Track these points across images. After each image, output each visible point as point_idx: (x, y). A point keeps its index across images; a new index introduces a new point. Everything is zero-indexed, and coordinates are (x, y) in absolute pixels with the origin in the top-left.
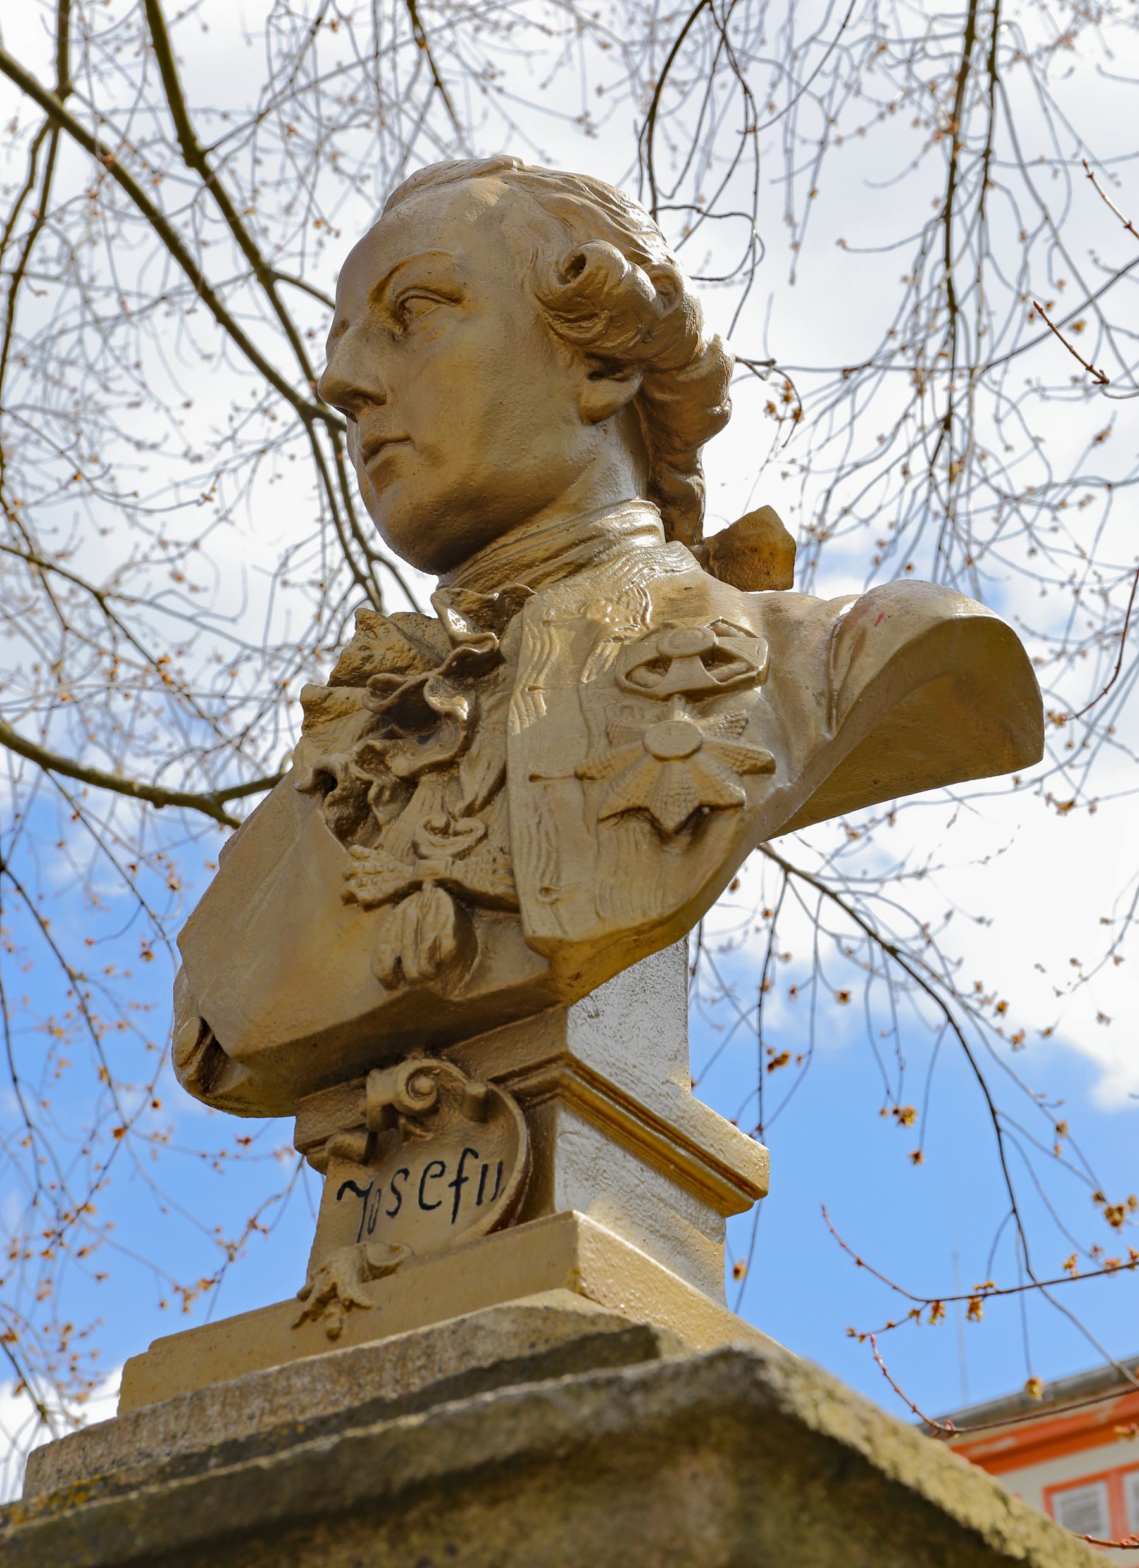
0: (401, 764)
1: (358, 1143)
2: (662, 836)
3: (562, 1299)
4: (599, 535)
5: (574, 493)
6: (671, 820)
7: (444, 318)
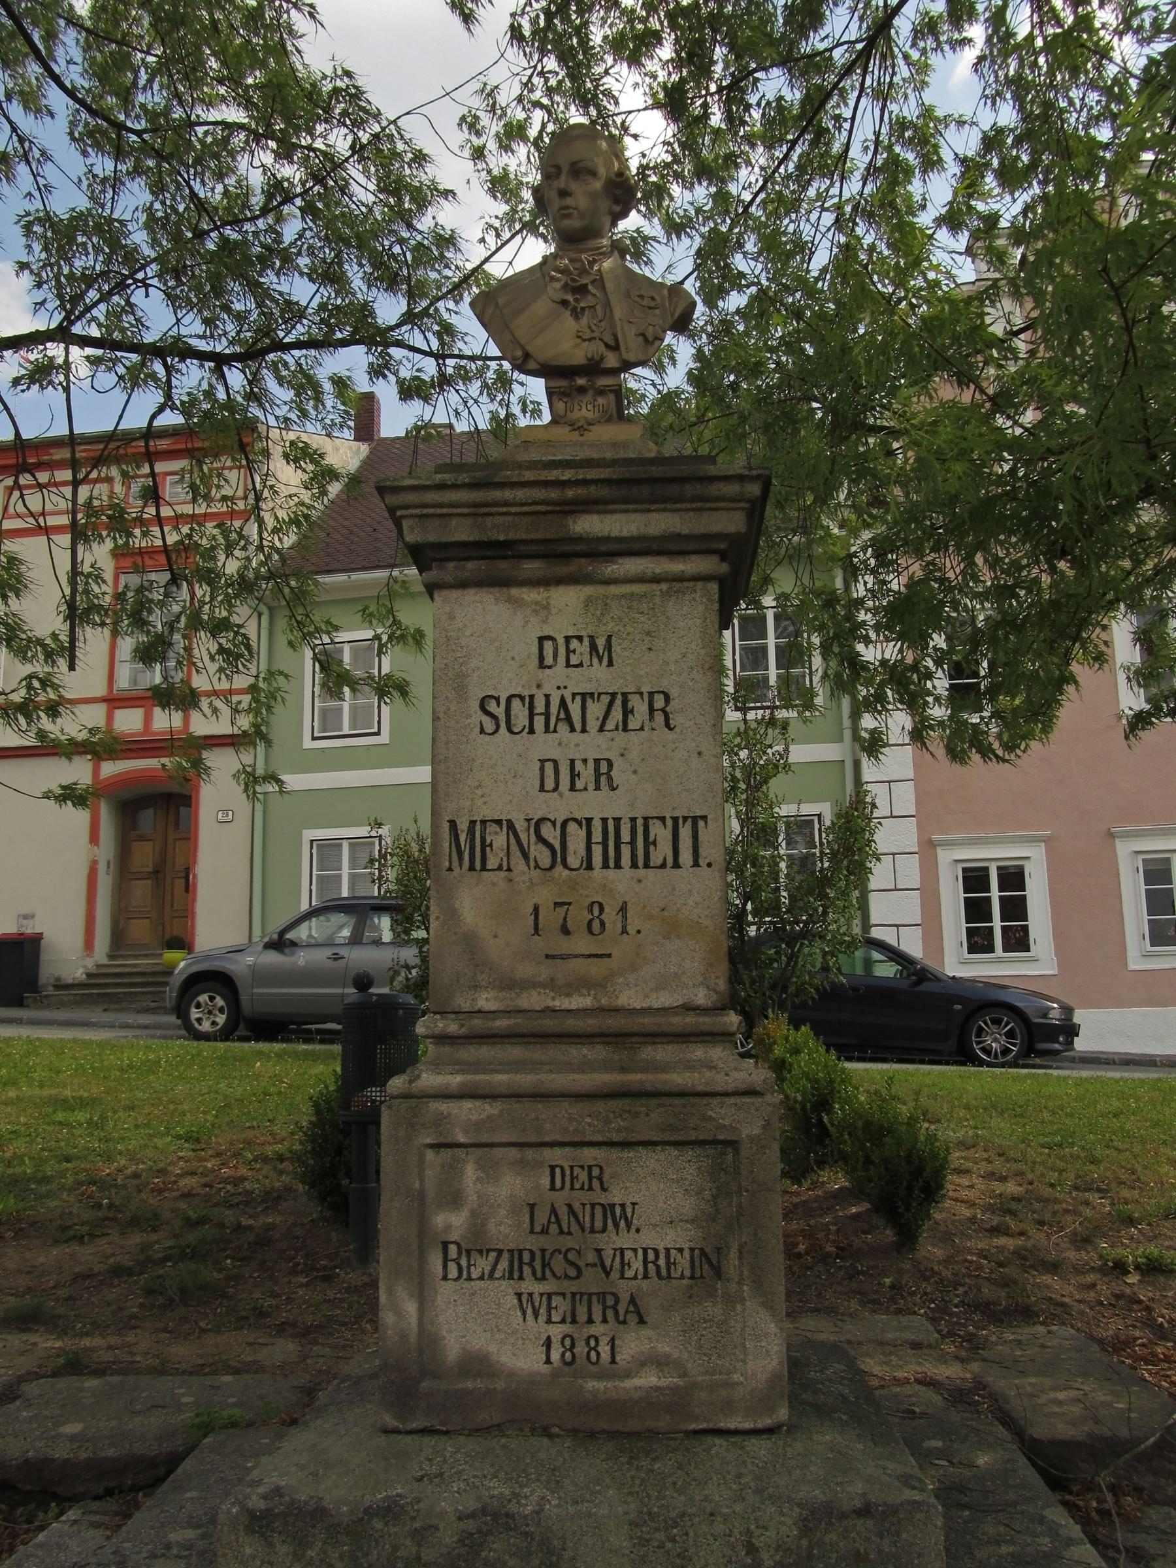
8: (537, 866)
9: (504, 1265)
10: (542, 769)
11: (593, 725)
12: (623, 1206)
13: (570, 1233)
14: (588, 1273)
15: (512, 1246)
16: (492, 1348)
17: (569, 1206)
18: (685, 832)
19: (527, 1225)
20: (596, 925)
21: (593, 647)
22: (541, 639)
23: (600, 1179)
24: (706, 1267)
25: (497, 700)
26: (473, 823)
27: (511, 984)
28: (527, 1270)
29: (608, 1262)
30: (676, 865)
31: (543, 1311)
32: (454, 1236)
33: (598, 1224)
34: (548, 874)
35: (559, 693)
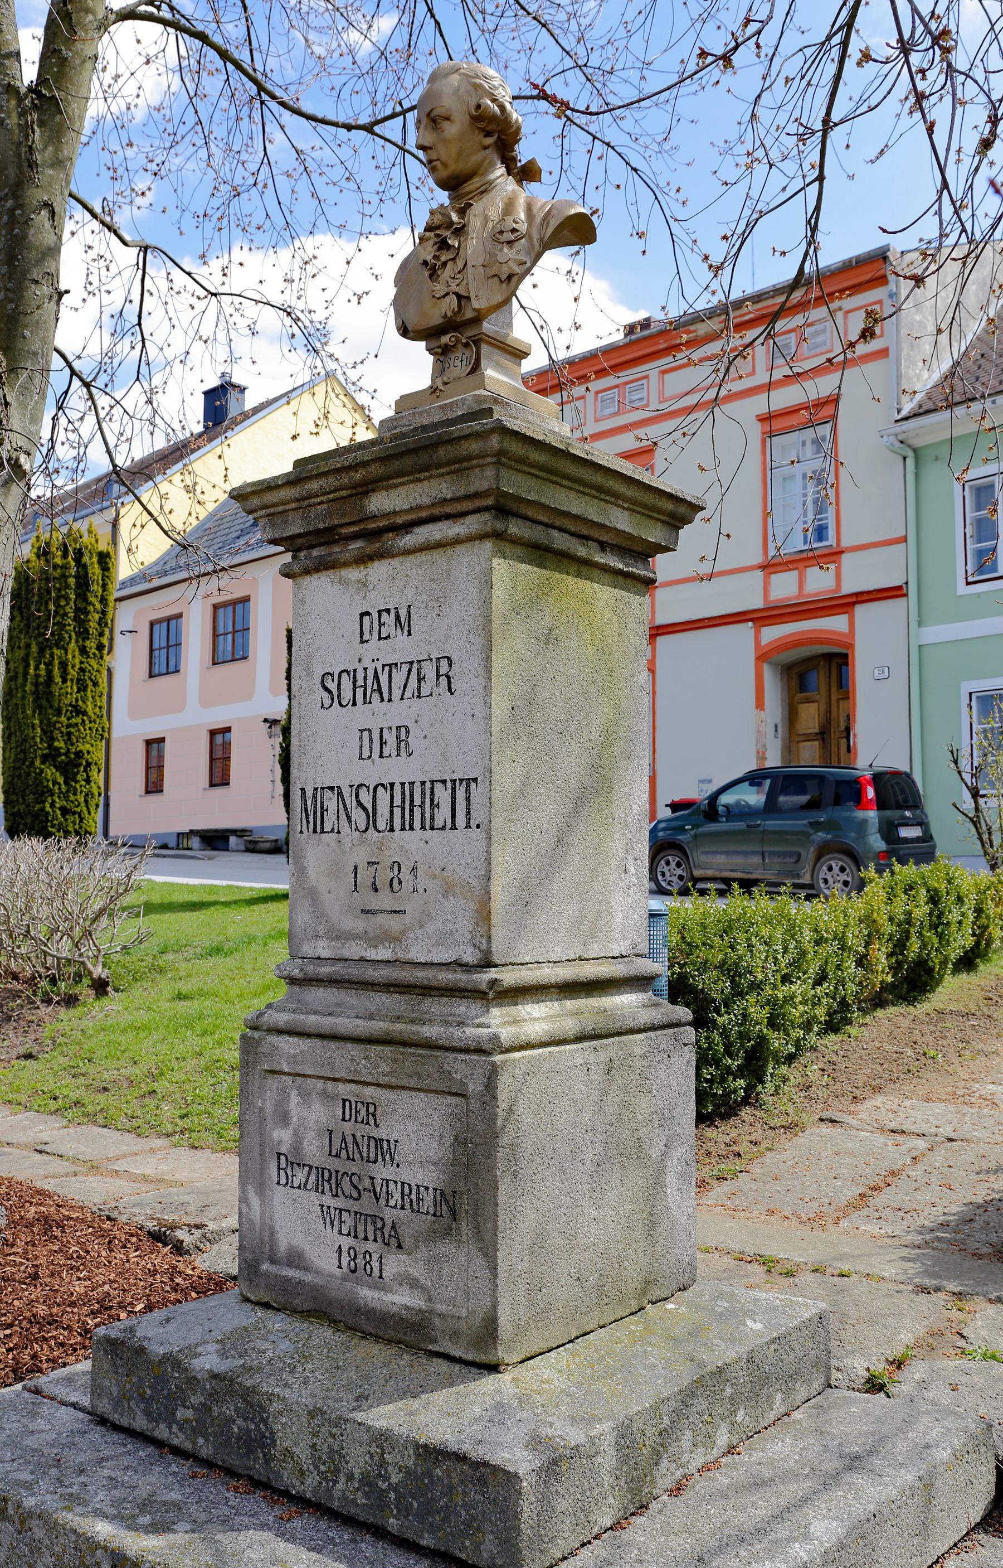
0: (443, 258)
1: (439, 350)
2: (501, 282)
3: (482, 392)
4: (490, 183)
5: (482, 170)
6: (504, 277)
7: (446, 125)
8: (357, 829)
9: (313, 1179)
10: (361, 738)
11: (396, 693)
12: (388, 1141)
13: (354, 1160)
14: (365, 1195)
15: (317, 1164)
16: (306, 1247)
17: (354, 1136)
18: (461, 794)
19: (327, 1148)
20: (395, 882)
21: (398, 618)
22: (362, 615)
23: (374, 1115)
24: (444, 1207)
25: (332, 675)
26: (316, 789)
27: (339, 936)
28: (326, 1186)
29: (378, 1191)
30: (454, 828)
31: (336, 1223)
32: (283, 1150)
33: (372, 1155)
34: (364, 835)
35: (374, 665)
